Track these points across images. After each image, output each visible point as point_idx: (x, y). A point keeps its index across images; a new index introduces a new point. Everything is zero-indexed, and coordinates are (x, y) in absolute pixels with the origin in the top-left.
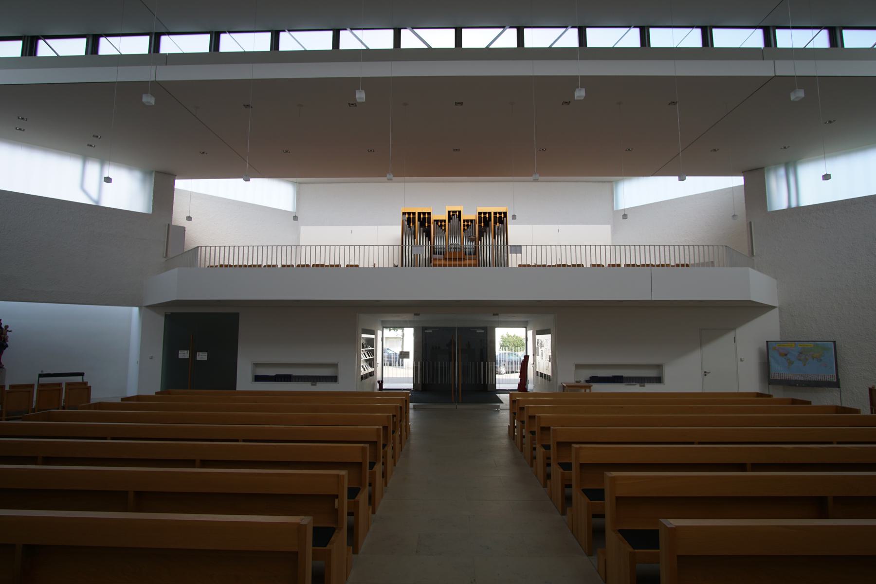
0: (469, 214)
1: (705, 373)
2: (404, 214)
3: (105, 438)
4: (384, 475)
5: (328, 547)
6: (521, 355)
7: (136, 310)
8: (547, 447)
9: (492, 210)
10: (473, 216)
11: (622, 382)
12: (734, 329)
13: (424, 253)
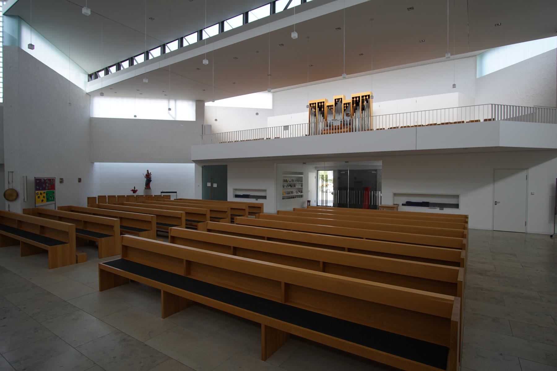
0: (348, 99)
1: (496, 203)
2: (310, 104)
9: (360, 95)
10: (349, 100)
11: (428, 206)
12: (527, 169)
13: (321, 126)
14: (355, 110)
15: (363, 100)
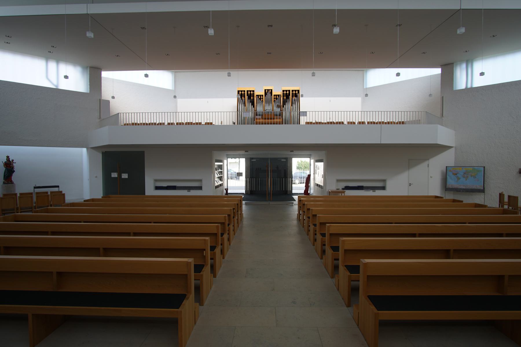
0: (278, 91)
1: (410, 185)
2: (239, 91)
3: (80, 222)
4: (229, 240)
5: (201, 273)
6: (308, 173)
7: (85, 150)
8: (315, 225)
9: (291, 89)
10: (280, 93)
12: (428, 159)
13: (250, 115)
14: (284, 103)
15: (292, 93)
